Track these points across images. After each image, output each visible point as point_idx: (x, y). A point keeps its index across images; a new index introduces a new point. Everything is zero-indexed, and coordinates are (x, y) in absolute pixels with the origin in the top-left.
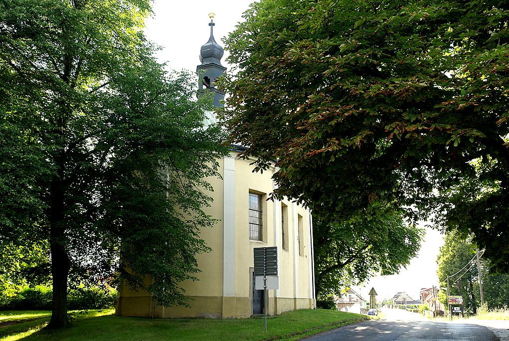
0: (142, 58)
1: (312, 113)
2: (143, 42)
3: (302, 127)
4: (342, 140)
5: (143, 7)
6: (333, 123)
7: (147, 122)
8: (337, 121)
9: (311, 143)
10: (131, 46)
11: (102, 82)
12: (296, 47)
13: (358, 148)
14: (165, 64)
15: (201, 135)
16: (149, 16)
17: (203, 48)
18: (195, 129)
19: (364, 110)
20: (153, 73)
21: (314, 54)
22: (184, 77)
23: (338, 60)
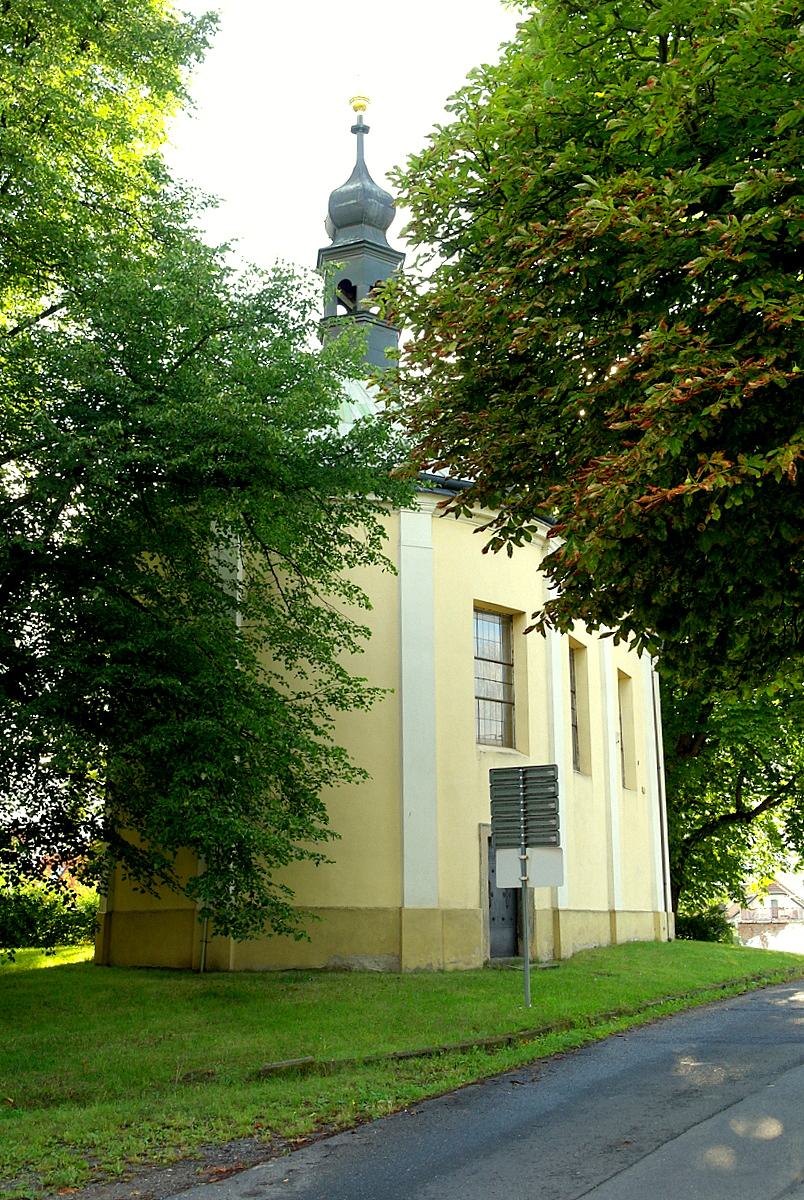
2: (163, 186)
3: (626, 425)
6: (715, 409)
10: (127, 197)
14: (225, 247)
15: (331, 448)
17: (335, 198)
18: (315, 433)
21: (658, 213)
22: (281, 283)
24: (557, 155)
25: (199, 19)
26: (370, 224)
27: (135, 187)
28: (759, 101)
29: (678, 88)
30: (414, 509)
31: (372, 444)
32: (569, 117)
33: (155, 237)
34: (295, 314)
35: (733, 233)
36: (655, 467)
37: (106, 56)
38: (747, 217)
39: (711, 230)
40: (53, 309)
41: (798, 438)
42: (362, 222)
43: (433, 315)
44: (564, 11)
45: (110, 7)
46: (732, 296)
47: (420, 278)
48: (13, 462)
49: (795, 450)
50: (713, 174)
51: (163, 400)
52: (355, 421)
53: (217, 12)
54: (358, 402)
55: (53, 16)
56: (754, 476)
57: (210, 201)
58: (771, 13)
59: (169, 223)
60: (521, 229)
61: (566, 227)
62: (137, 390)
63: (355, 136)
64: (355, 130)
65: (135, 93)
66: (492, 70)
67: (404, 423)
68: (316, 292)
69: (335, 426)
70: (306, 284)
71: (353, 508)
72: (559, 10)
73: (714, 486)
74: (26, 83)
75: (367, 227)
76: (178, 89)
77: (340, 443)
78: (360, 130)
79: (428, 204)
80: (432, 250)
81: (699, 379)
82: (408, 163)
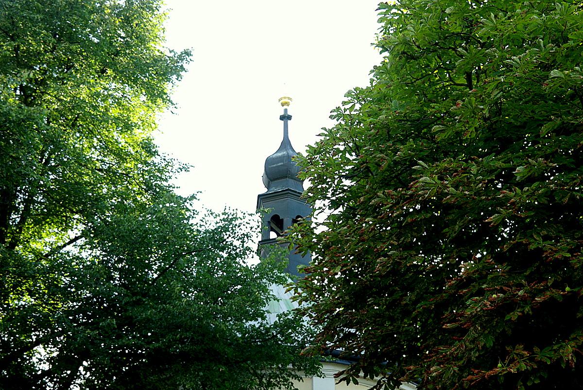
0: (149, 187)
1: (472, 295)
2: (153, 158)
3: (454, 325)
4: (536, 349)
5: (153, 95)
6: (514, 316)
7: (155, 314)
8: (523, 312)
9: (474, 355)
10: (129, 165)
11: (72, 234)
12: (432, 173)
13: (571, 367)
14: (193, 197)
15: (263, 334)
16: (165, 110)
17: (269, 162)
18: (252, 323)
19: (576, 290)
20: (170, 216)
21: (467, 185)
22: (229, 222)
23: (515, 195)
24: (402, 147)
25: (180, 54)
26: (292, 178)
27: (134, 159)
28: (533, 112)
29: (476, 108)
30: (320, 377)
31: (290, 331)
32: (409, 123)
33: (146, 191)
34: (237, 243)
35: (517, 199)
36: (477, 355)
37: (118, 77)
38: (526, 189)
39: (503, 197)
40: (76, 238)
41: (575, 336)
42: (286, 177)
43: (329, 246)
44: (404, 58)
45: (122, 47)
46: (521, 239)
47: (316, 223)
48: (41, 346)
49: (573, 345)
50: (503, 160)
51: (146, 302)
52: (278, 316)
53: (190, 49)
54: (281, 301)
55: (84, 54)
56: (546, 363)
57: (183, 167)
58: (533, 63)
59: (156, 182)
60: (380, 194)
61: (410, 192)
62: (128, 296)
63: (282, 122)
64: (282, 118)
65: (138, 100)
66: (362, 91)
67: (311, 316)
68: (251, 228)
69: (264, 318)
70: (245, 223)
71: (277, 376)
72: (400, 58)
73: (518, 370)
74: (64, 97)
75: (291, 180)
76: (165, 96)
77: (268, 330)
78: (285, 118)
79: (320, 176)
80: (324, 205)
81: (501, 295)
82: (307, 151)
